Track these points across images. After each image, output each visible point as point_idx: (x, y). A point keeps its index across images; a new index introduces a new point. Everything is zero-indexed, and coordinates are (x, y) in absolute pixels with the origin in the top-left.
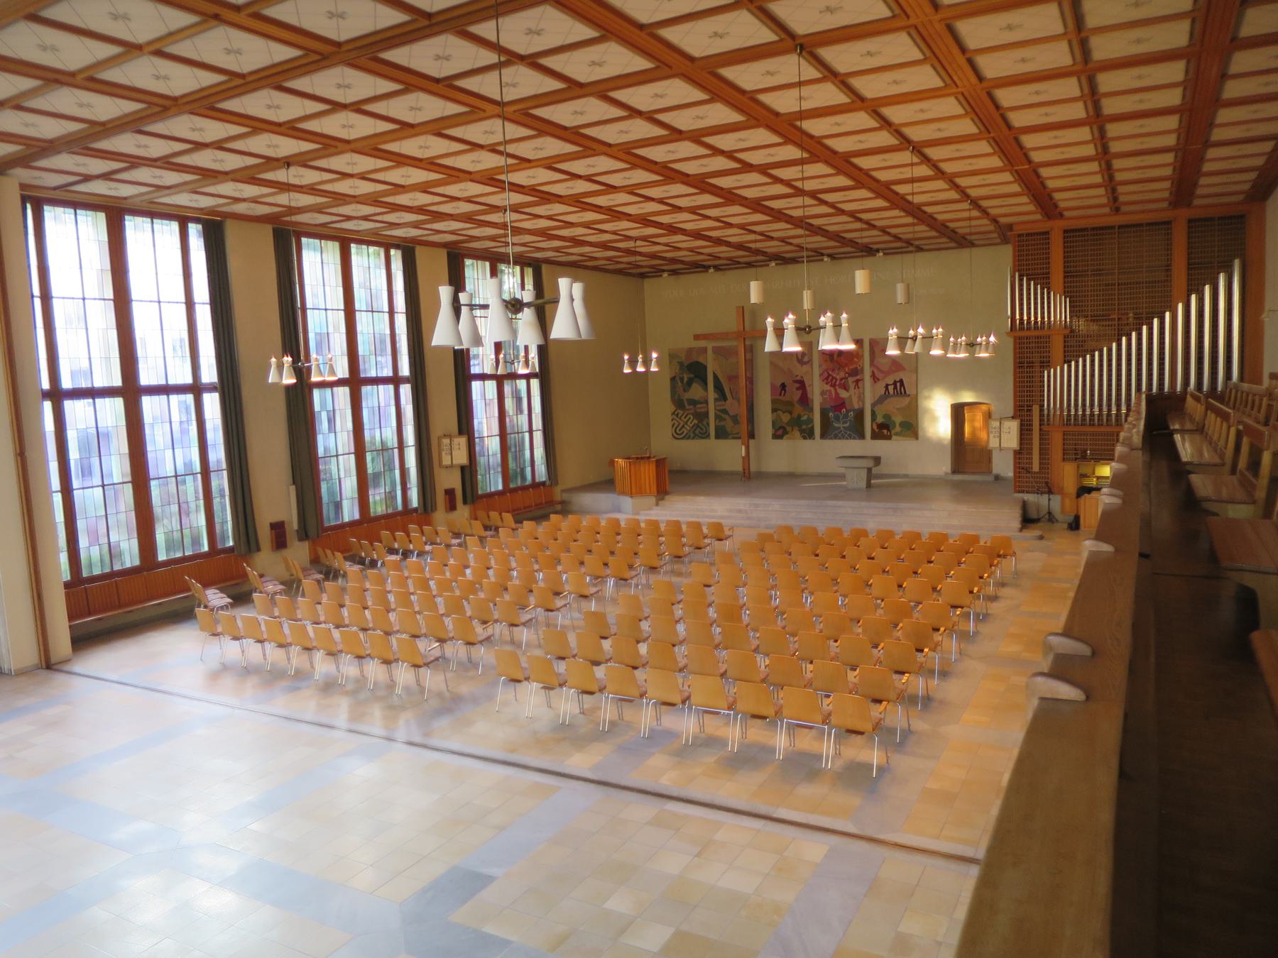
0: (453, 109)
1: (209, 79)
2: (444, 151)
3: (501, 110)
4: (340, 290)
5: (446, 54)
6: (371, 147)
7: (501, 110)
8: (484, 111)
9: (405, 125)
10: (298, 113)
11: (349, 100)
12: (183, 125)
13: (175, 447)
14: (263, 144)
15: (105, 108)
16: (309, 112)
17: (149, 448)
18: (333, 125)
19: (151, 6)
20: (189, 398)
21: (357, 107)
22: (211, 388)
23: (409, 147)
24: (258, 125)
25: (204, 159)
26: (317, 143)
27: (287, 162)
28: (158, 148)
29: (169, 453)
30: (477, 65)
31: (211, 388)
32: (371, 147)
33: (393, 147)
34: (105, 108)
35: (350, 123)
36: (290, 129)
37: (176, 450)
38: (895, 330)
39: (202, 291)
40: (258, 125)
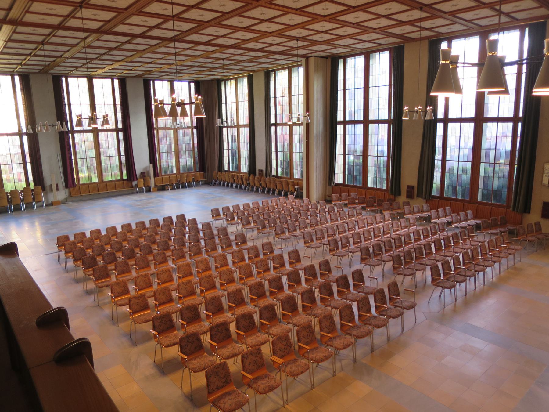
0: (306, 19)
1: (216, 15)
2: (353, 43)
3: (325, 18)
4: (370, 97)
5: (326, 8)
6: (278, 34)
7: (325, 18)
8: (318, 19)
9: (289, 26)
10: (250, 24)
11: (266, 18)
12: (211, 30)
13: (379, 145)
14: (239, 35)
15: (186, 26)
16: (310, 34)
17: (369, 144)
18: (263, 27)
19: (231, 2)
20: (115, 133)
21: (269, 20)
22: (121, 130)
23: (294, 33)
24: (236, 29)
25: (221, 41)
26: (308, 42)
27: (298, 48)
28: (205, 39)
29: (376, 147)
30: (309, 3)
31: (121, 130)
32: (278, 34)
33: (287, 33)
34: (186, 26)
35: (300, 32)
36: (247, 29)
37: (379, 146)
38: (407, 107)
39: (340, 94)
40: (236, 29)
